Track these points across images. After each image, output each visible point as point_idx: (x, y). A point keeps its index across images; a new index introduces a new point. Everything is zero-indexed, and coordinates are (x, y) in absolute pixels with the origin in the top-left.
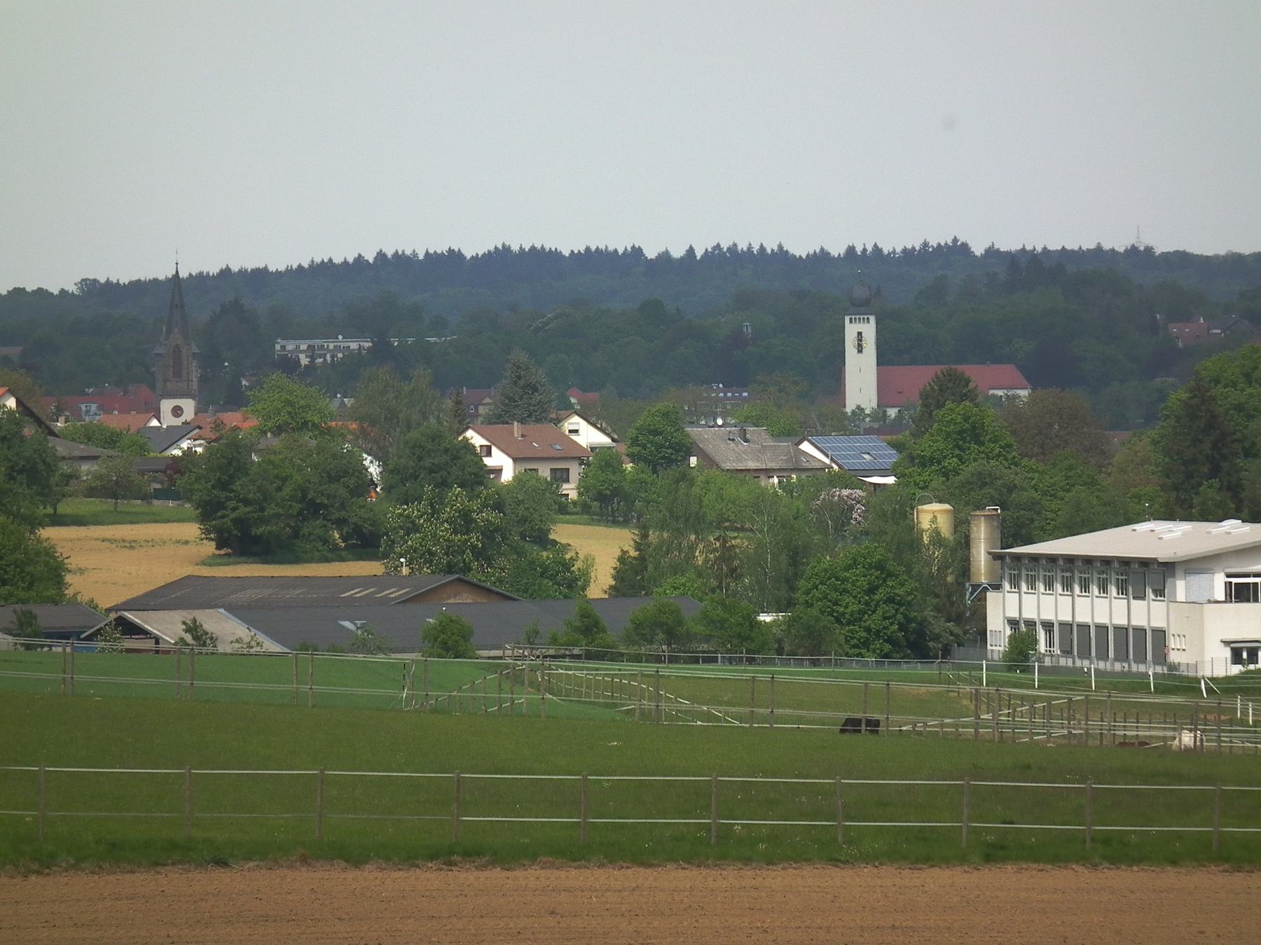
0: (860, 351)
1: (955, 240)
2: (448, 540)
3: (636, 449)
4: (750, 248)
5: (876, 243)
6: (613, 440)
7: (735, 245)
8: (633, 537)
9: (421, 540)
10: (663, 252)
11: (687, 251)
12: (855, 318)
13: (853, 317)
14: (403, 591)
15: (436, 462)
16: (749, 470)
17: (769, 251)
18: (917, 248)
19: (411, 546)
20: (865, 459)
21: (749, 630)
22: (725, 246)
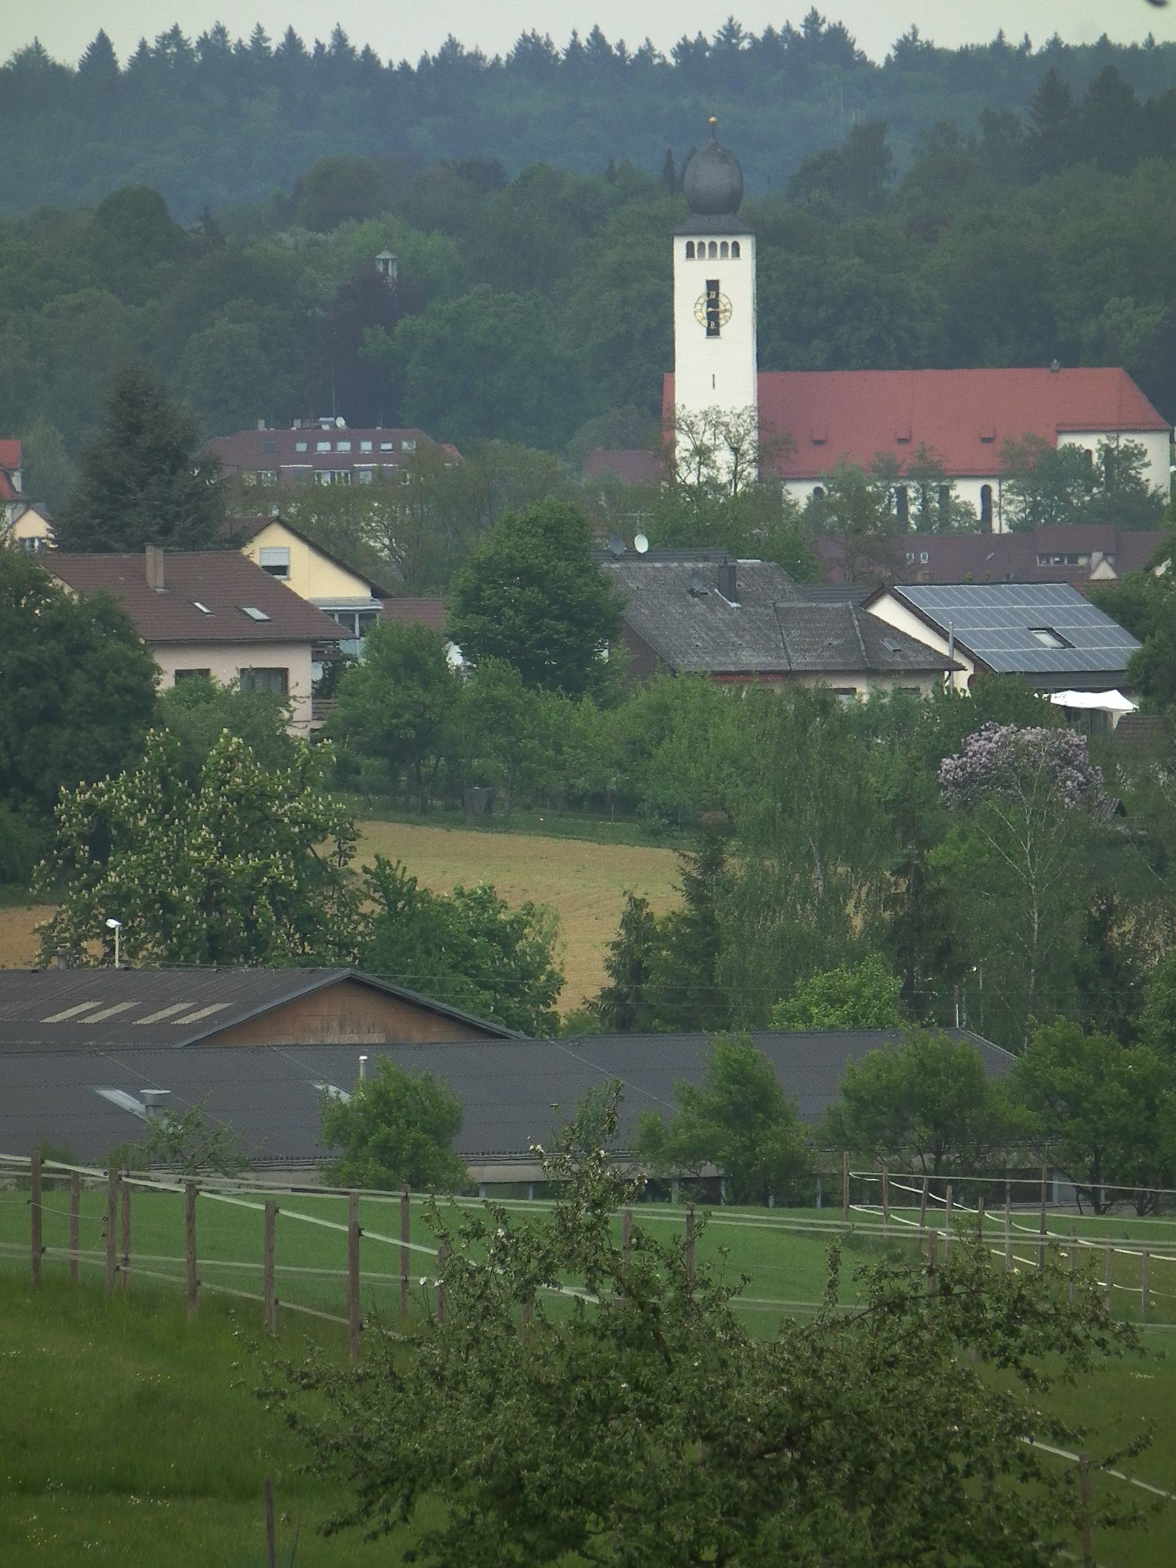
0: (713, 332)
1: (813, 20)
2: (211, 873)
3: (475, 622)
4: (259, 37)
5: (597, 28)
6: (377, 593)
7: (220, 31)
8: (684, 865)
9: (141, 871)
10: (29, 51)
11: (93, 48)
12: (702, 245)
13: (696, 241)
14: (206, 1012)
15: (32, 658)
16: (747, 673)
17: (310, 48)
18: (711, 42)
19: (117, 887)
20: (1043, 645)
21: (1147, 1119)
22: (192, 34)
